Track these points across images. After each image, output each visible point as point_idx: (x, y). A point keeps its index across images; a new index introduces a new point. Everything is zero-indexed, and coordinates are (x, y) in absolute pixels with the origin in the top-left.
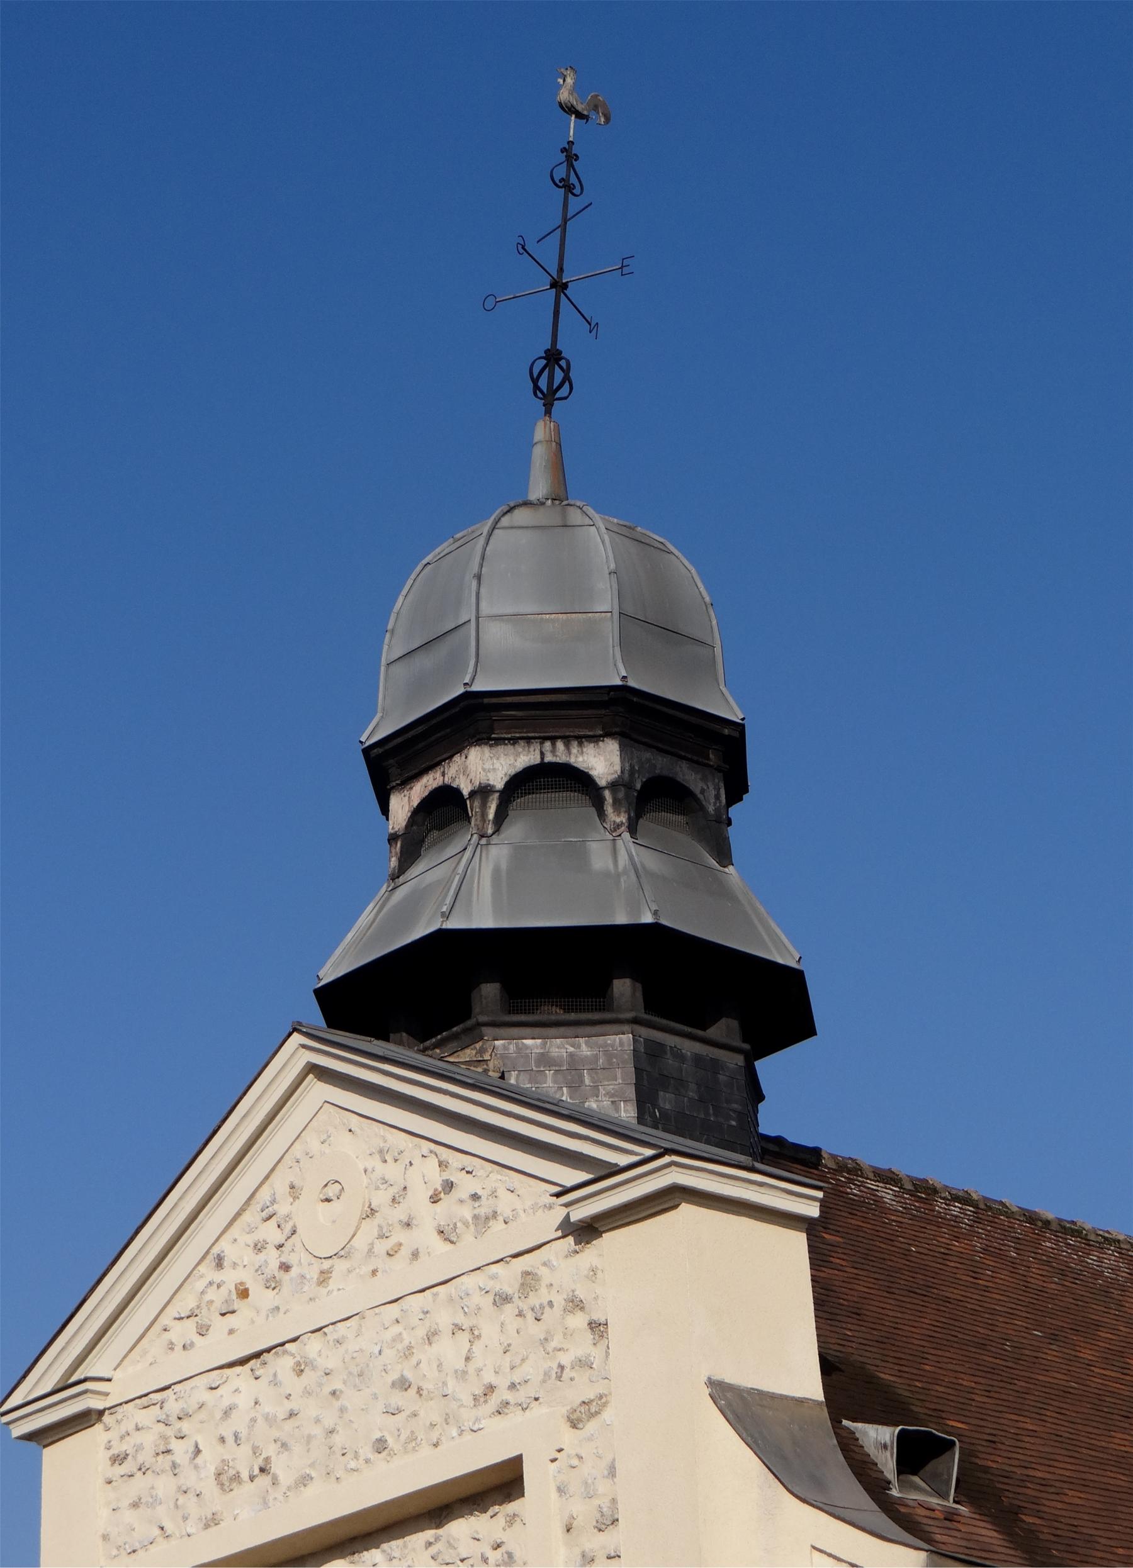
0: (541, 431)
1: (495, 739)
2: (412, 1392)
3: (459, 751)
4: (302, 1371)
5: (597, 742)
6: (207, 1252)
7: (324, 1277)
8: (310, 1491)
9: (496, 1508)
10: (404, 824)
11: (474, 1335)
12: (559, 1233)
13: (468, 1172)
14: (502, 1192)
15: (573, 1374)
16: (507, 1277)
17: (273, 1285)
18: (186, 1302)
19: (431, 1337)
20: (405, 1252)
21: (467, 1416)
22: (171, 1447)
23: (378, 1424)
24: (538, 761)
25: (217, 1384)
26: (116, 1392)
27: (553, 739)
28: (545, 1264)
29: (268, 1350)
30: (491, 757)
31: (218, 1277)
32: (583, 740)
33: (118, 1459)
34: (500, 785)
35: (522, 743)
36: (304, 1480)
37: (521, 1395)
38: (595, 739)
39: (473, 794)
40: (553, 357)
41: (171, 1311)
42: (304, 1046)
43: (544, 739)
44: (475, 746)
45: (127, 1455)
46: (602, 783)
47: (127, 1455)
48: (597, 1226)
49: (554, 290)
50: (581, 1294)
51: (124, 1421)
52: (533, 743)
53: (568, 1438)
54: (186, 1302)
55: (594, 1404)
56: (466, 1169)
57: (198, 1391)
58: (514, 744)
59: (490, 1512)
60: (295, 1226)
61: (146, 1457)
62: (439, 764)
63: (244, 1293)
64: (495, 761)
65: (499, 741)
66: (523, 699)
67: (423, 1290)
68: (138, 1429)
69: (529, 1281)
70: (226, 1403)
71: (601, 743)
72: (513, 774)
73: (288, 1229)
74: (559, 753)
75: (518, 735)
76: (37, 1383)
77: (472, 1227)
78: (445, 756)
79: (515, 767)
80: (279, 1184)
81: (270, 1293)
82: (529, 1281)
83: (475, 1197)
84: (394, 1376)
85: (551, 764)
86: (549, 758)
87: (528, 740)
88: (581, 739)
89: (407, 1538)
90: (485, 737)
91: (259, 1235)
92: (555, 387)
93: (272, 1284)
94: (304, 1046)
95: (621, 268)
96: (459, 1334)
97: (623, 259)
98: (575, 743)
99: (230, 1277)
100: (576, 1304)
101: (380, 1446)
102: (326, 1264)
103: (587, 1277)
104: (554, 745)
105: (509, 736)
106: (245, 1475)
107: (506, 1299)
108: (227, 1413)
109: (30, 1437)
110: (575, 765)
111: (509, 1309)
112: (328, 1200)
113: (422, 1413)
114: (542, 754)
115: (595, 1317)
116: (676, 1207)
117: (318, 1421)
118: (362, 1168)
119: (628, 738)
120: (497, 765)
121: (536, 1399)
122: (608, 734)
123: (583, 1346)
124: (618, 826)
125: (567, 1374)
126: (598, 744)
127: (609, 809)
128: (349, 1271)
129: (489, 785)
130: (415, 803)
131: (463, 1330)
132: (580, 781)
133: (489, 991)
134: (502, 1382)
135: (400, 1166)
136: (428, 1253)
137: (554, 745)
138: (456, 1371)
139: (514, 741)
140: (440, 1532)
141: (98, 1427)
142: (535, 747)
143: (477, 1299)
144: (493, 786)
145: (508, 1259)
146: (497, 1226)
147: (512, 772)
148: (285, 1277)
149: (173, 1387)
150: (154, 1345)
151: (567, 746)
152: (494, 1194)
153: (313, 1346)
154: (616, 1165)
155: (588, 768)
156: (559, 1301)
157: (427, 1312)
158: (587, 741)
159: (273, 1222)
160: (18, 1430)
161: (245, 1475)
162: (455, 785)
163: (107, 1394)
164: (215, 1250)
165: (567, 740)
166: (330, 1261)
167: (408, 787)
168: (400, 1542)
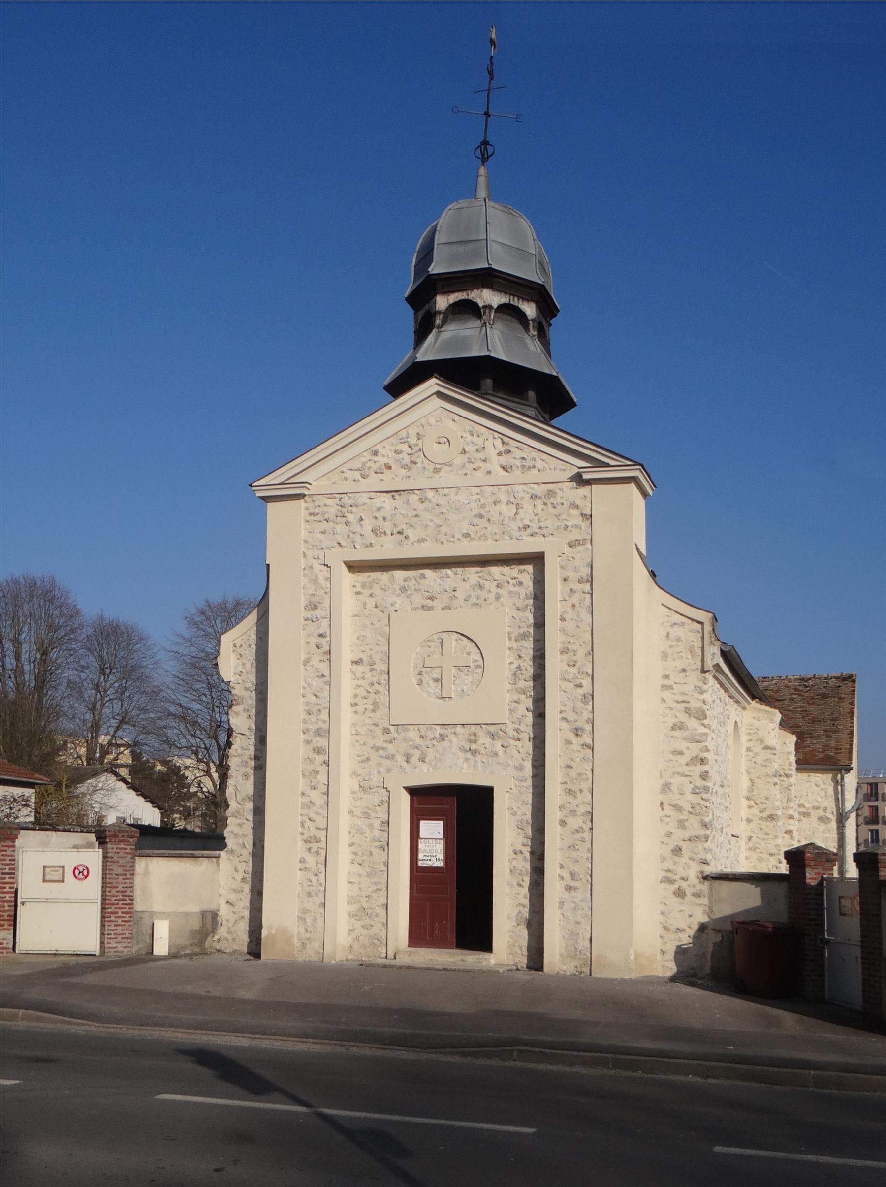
0: (482, 171)
3: (478, 289)
6: (370, 448)
7: (437, 471)
8: (424, 544)
9: (515, 566)
10: (445, 309)
11: (518, 506)
12: (569, 480)
14: (538, 459)
15: (572, 529)
21: (516, 534)
23: (465, 528)
24: (508, 302)
26: (312, 490)
27: (514, 296)
28: (560, 489)
29: (403, 491)
33: (313, 514)
34: (495, 306)
35: (503, 293)
36: (422, 540)
38: (528, 301)
40: (485, 143)
41: (348, 466)
42: (437, 384)
43: (511, 295)
46: (529, 318)
53: (567, 550)
57: (363, 498)
59: (512, 567)
61: (331, 515)
62: (466, 290)
66: (506, 277)
67: (493, 486)
68: (325, 505)
69: (551, 494)
74: (515, 302)
76: (275, 478)
77: (520, 469)
78: (468, 288)
82: (551, 494)
83: (523, 458)
85: (512, 305)
86: (512, 302)
87: (506, 293)
88: (524, 299)
89: (466, 569)
90: (490, 287)
94: (437, 384)
95: (517, 118)
96: (510, 505)
99: (381, 460)
101: (467, 535)
102: (438, 466)
104: (514, 298)
106: (389, 532)
109: (263, 498)
111: (539, 503)
112: (439, 443)
113: (489, 528)
114: (510, 300)
116: (630, 483)
118: (460, 435)
119: (539, 307)
120: (495, 299)
121: (552, 534)
122: (533, 301)
123: (579, 521)
124: (534, 336)
127: (531, 328)
128: (451, 471)
130: (452, 302)
132: (520, 316)
133: (489, 382)
137: (514, 298)
138: (510, 517)
139: (500, 291)
140: (483, 569)
141: (302, 500)
142: (508, 296)
143: (522, 494)
147: (500, 303)
151: (518, 300)
152: (534, 459)
154: (608, 464)
156: (567, 503)
160: (259, 494)
161: (389, 532)
162: (475, 301)
163: (309, 489)
164: (374, 449)
165: (519, 298)
166: (440, 466)
168: (462, 569)
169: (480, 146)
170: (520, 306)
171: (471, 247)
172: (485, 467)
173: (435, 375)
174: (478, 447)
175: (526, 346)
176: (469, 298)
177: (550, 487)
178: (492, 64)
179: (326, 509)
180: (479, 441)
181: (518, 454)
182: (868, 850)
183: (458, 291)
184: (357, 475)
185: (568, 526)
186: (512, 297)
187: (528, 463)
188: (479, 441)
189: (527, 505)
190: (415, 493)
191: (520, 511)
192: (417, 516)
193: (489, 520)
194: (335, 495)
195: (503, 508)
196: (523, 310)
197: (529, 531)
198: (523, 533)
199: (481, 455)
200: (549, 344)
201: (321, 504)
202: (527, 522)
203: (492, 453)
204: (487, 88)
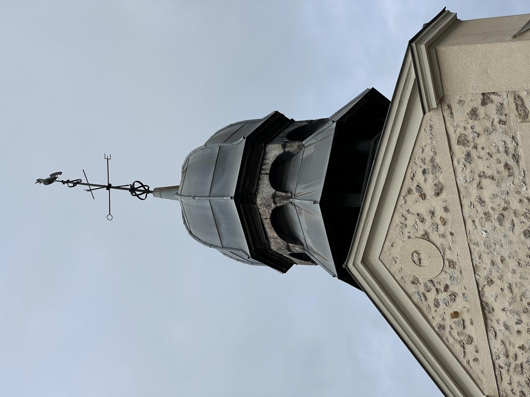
1: (256, 192)
2: (505, 213)
4: (491, 280)
5: (266, 153)
7: (452, 264)
11: (482, 175)
13: (414, 176)
16: (460, 151)
17: (454, 297)
18: (458, 348)
19: (482, 202)
20: (444, 215)
22: (519, 363)
24: (268, 176)
25: (494, 332)
27: (261, 169)
30: (262, 193)
31: (448, 329)
32: (264, 158)
34: (274, 191)
35: (260, 181)
37: (511, 145)
38: (265, 153)
39: (275, 203)
40: (133, 190)
43: (260, 173)
44: (257, 200)
45: (521, 391)
46: (282, 151)
47: (521, 391)
48: (441, 97)
49: (111, 189)
50: (469, 110)
51: (507, 392)
52: (261, 177)
54: (458, 348)
55: (518, 103)
56: (412, 177)
58: (259, 185)
60: (429, 281)
63: (456, 314)
64: (264, 192)
65: (257, 190)
70: (503, 328)
71: (267, 152)
72: (271, 186)
73: (430, 285)
75: (256, 183)
78: (259, 218)
79: (268, 184)
80: (411, 289)
81: (457, 299)
84: (497, 224)
86: (268, 172)
87: (259, 179)
91: (431, 302)
92: (144, 189)
93: (454, 296)
97: (105, 158)
98: (265, 161)
100: (474, 113)
102: (447, 263)
103: (462, 106)
104: (263, 169)
105: (256, 186)
107: (468, 155)
108: (507, 327)
110: (273, 162)
111: (474, 153)
114: (266, 174)
115: (480, 102)
117: (514, 272)
119: (270, 140)
123: (492, 108)
124: (299, 146)
125: (503, 118)
126: (267, 153)
129: (272, 195)
131: (480, 182)
134: (504, 158)
135: (409, 216)
136: (446, 201)
137: (263, 169)
139: (258, 184)
142: (262, 176)
144: (273, 193)
145: (452, 153)
146: (438, 160)
147: (270, 186)
148: (452, 289)
149: (494, 360)
150: (476, 368)
151: (265, 164)
153: (483, 274)
154: (415, 80)
155: (275, 157)
157: (471, 203)
158: (265, 156)
159: (427, 294)
165: (263, 164)
166: (446, 261)
167: (270, 239)
169: (138, 196)
170: (271, 163)
171: (219, 216)
172: (440, 213)
173: (344, 266)
174: (418, 221)
175: (310, 157)
176: (269, 217)
177: (454, 142)
178: (68, 182)
179: (515, 385)
180: (411, 220)
181: (420, 177)
182: (473, 252)
183: (264, 228)
184: (469, 348)
185: (500, 121)
186: (263, 172)
187: (428, 166)
188: (411, 220)
189: (481, 166)
190: (482, 289)
191: (489, 173)
192: (510, 288)
193: (505, 209)
194: (497, 374)
195: (486, 195)
196: (274, 159)
197: (512, 163)
198: (516, 170)
199: (427, 217)
200: (311, 122)
201: (509, 388)
202: (501, 167)
203: (422, 208)
204: (88, 186)
